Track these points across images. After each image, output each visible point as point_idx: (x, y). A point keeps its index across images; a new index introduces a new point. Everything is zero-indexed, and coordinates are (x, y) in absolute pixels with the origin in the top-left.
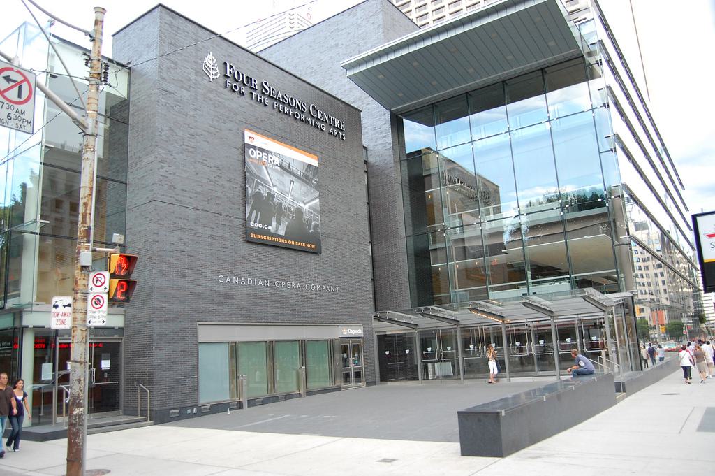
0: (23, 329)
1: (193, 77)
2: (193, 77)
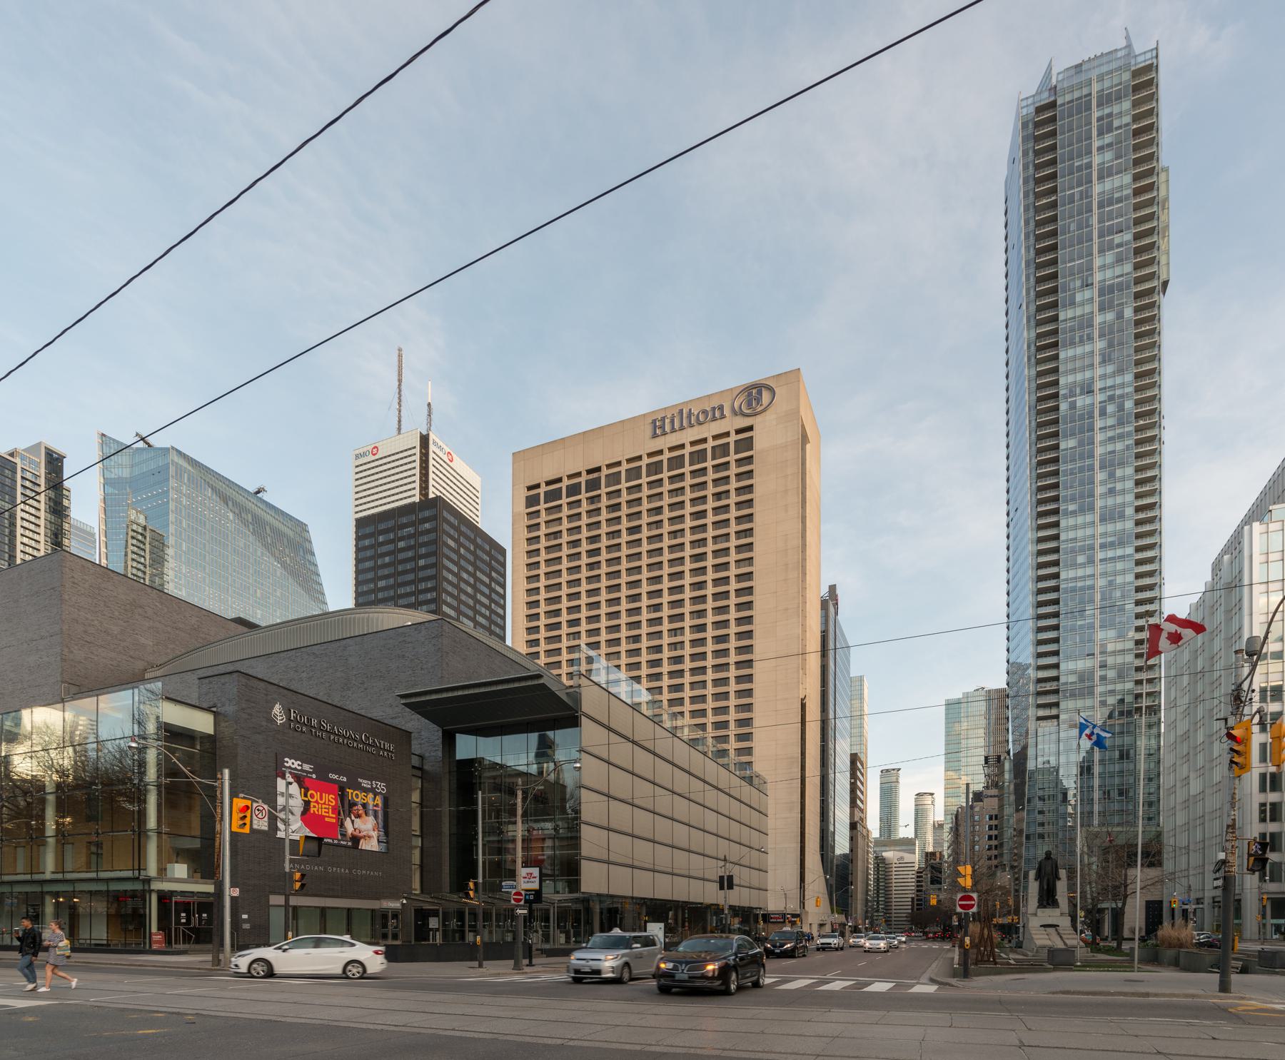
0: (151, 891)
1: (264, 723)
2: (264, 723)
